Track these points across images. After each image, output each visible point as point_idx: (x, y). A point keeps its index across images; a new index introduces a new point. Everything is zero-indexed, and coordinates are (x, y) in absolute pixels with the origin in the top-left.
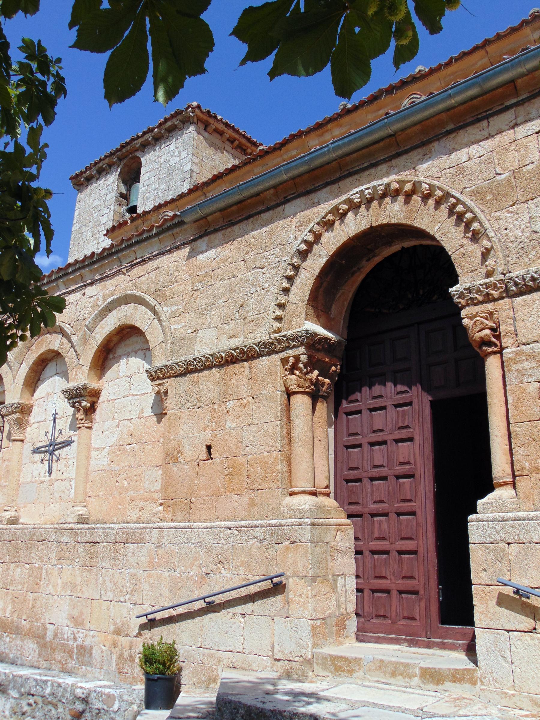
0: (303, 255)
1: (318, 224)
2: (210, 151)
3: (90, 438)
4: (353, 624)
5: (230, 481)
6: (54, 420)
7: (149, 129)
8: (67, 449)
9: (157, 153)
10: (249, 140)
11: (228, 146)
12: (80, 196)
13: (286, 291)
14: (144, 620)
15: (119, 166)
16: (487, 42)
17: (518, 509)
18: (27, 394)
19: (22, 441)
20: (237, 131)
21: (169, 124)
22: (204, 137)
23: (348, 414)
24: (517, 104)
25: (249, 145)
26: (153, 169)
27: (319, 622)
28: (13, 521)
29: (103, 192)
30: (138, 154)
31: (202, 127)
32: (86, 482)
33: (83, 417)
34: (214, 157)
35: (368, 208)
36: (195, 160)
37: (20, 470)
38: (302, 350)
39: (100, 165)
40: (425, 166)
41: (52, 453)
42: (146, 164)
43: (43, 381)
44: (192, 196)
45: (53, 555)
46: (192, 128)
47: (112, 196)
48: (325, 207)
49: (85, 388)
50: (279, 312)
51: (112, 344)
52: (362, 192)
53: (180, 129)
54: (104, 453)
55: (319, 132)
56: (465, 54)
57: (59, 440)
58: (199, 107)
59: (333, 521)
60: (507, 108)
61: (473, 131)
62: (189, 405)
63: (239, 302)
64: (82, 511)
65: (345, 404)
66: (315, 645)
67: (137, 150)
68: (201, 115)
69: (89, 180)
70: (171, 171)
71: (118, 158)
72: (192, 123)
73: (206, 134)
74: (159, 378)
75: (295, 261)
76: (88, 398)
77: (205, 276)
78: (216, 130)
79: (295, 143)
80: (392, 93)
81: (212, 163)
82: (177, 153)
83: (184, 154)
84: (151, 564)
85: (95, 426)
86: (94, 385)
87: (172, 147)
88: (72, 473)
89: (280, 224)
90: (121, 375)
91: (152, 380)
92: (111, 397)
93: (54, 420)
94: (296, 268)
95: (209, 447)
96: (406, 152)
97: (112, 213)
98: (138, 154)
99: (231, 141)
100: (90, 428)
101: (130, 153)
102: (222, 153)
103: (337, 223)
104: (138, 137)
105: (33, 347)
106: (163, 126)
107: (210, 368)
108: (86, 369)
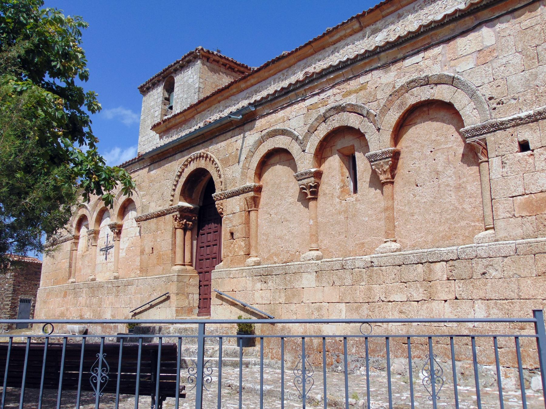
0: (179, 176)
1: (183, 165)
2: (210, 74)
3: (119, 245)
4: (197, 311)
5: (158, 261)
6: (107, 237)
7: (177, 61)
8: (112, 249)
9: (182, 75)
10: (236, 63)
11: (223, 69)
12: (144, 99)
13: (174, 190)
14: (132, 313)
15: (163, 82)
16: (310, 43)
17: (223, 268)
18: (97, 226)
19: (96, 246)
20: (228, 59)
21: (187, 59)
22: (207, 66)
23: (202, 235)
24: (233, 129)
25: (236, 66)
26: (180, 85)
27: (179, 309)
28: (93, 280)
29: (156, 97)
30: (173, 75)
31: (206, 60)
32: (118, 263)
33: (116, 236)
34: (214, 77)
35: (196, 161)
36: (201, 80)
37: (96, 259)
38: (178, 213)
39: (154, 81)
40: (211, 147)
41: (107, 251)
42: (177, 82)
43: (104, 220)
44: (190, 110)
45: (106, 292)
46: (199, 62)
47: (160, 100)
48: (185, 158)
49: (116, 224)
50: (172, 198)
51: (126, 205)
52: (194, 155)
53: (194, 62)
54: (124, 251)
55: (245, 80)
56: (301, 48)
57: (109, 246)
58: (202, 49)
59: (188, 275)
60: (230, 131)
61: (222, 137)
62: (147, 232)
63: (162, 193)
64: (116, 274)
65: (201, 231)
66: (177, 316)
67: (172, 73)
68: (204, 54)
69: (148, 89)
70: (189, 86)
71: (163, 77)
72: (199, 59)
73: (208, 64)
74: (138, 221)
75: (177, 179)
76: (117, 228)
77: (152, 180)
78: (214, 60)
79: (234, 86)
80: (274, 63)
81: (212, 81)
82: (192, 76)
83: (195, 77)
84: (135, 293)
85: (121, 240)
86: (119, 222)
87: (190, 72)
88: (113, 260)
89: (174, 163)
90: (130, 218)
91: (137, 222)
92: (127, 228)
93: (107, 237)
94: (177, 181)
95: (153, 248)
96: (207, 141)
97: (160, 110)
98: (173, 75)
99: (224, 65)
100: (119, 240)
101: (169, 74)
102: (219, 74)
103: (189, 165)
104: (172, 66)
105: (98, 205)
106: (184, 60)
107: (153, 218)
108: (116, 216)
